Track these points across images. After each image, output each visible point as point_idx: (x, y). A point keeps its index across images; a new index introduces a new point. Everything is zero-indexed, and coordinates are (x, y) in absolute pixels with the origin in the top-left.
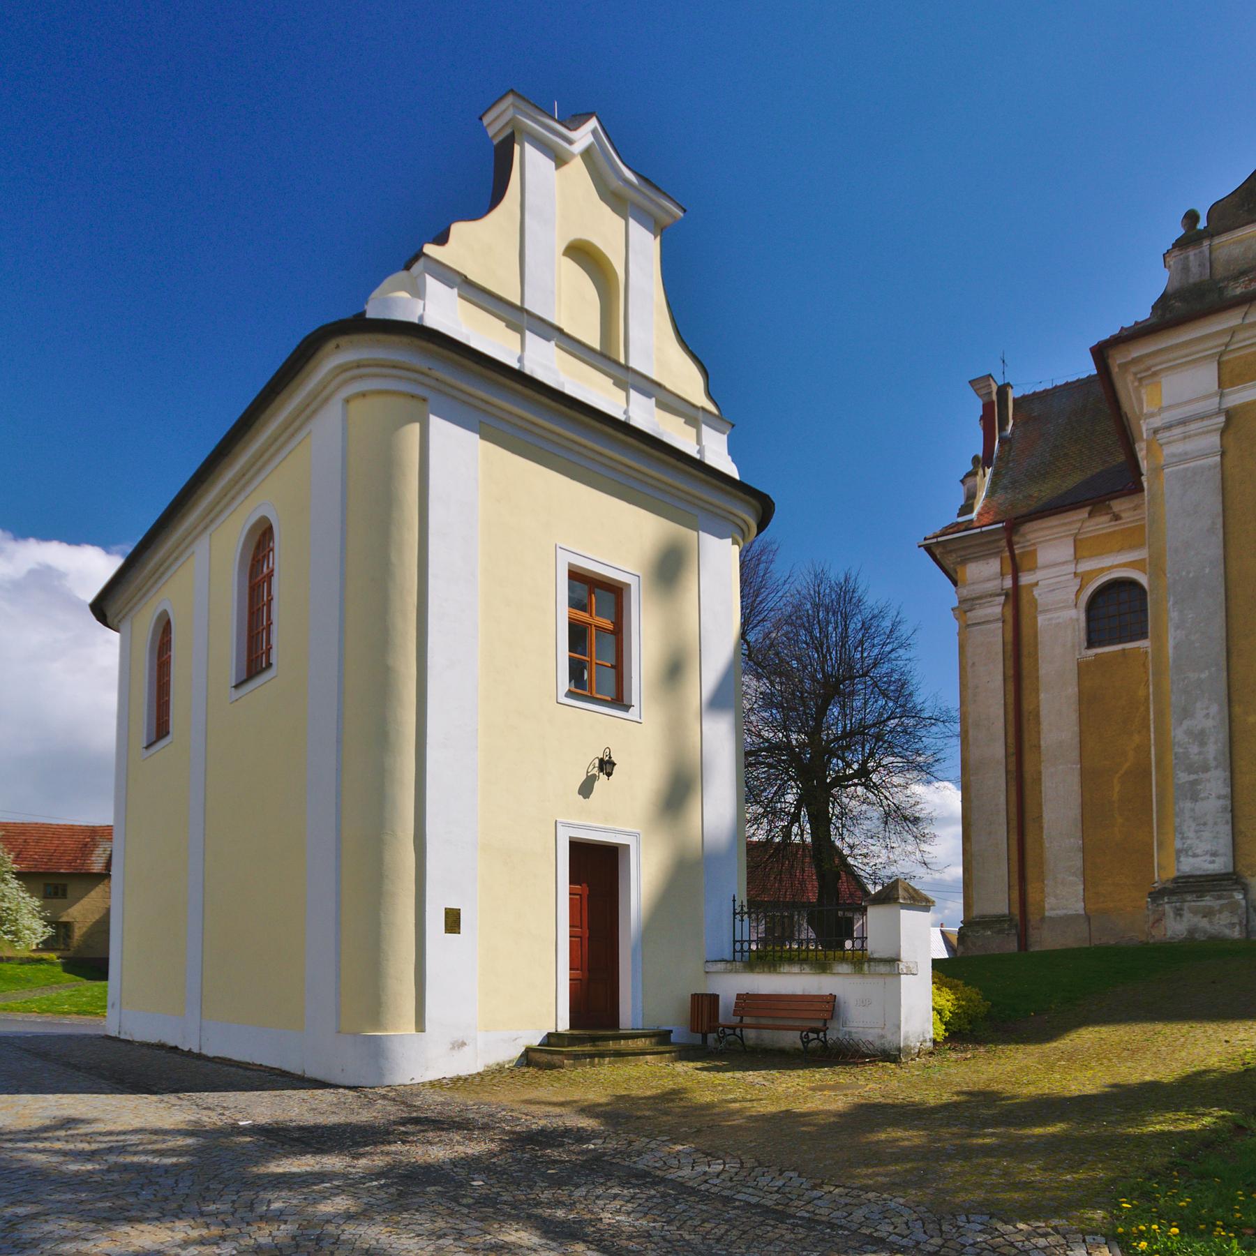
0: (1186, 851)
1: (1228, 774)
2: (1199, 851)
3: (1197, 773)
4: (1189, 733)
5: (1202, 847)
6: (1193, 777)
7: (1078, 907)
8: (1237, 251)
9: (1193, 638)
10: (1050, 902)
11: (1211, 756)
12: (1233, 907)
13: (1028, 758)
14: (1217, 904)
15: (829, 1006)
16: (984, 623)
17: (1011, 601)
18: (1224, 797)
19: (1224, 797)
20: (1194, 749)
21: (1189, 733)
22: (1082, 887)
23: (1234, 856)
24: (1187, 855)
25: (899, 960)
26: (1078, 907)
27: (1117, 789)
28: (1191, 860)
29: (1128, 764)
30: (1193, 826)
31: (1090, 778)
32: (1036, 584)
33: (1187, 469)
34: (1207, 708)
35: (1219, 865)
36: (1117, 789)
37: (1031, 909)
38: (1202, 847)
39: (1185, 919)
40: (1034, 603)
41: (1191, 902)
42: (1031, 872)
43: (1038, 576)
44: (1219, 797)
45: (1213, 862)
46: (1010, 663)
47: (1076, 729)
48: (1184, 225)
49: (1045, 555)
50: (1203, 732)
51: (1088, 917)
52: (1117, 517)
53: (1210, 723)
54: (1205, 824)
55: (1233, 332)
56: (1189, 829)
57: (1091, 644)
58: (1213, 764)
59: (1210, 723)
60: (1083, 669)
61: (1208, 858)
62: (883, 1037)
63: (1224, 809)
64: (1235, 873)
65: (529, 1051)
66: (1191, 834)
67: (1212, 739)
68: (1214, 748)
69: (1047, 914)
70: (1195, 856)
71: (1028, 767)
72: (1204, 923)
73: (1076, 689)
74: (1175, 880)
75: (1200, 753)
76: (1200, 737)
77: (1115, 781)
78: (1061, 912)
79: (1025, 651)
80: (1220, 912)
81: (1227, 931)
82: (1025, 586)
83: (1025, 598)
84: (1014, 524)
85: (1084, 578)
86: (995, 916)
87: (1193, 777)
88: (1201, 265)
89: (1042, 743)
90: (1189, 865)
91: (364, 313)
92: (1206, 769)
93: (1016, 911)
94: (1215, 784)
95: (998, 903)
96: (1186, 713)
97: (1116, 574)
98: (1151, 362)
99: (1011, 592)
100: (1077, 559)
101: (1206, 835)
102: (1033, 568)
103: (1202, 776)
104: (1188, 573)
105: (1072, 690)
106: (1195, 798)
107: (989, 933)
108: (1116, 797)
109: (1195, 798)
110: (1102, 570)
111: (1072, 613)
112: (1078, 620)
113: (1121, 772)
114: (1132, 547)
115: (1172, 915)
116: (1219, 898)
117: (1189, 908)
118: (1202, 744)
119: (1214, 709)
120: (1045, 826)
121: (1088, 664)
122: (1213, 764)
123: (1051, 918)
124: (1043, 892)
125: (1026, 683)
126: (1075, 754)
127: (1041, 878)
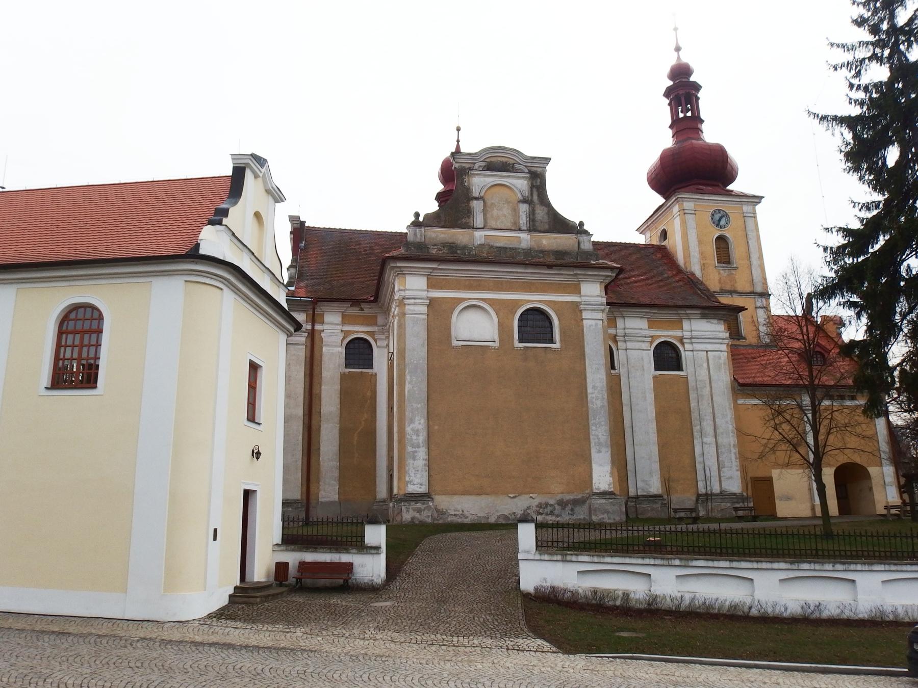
0: (411, 482)
1: (427, 450)
2: (415, 483)
3: (415, 448)
4: (412, 430)
5: (416, 481)
6: (414, 449)
7: (335, 497)
8: (434, 235)
9: (415, 389)
10: (322, 494)
11: (421, 442)
12: (429, 508)
13: (314, 417)
14: (423, 507)
15: (349, 567)
16: (296, 344)
17: (310, 335)
18: (426, 460)
19: (426, 460)
20: (414, 437)
21: (412, 430)
22: (338, 487)
23: (429, 486)
24: (411, 484)
25: (380, 548)
26: (335, 497)
27: (356, 439)
28: (412, 487)
29: (361, 428)
30: (413, 471)
31: (345, 433)
32: (323, 331)
33: (414, 317)
34: (420, 420)
35: (423, 489)
36: (356, 439)
37: (312, 497)
38: (416, 481)
39: (410, 513)
40: (322, 339)
41: (413, 505)
42: (312, 478)
43: (325, 327)
44: (423, 460)
45: (421, 488)
46: (308, 367)
47: (339, 407)
48: (414, 216)
49: (328, 318)
50: (418, 430)
51: (340, 502)
52: (362, 310)
53: (420, 427)
54: (418, 471)
55: (434, 269)
56: (412, 472)
57: (347, 366)
58: (421, 445)
59: (420, 427)
60: (343, 377)
61: (419, 486)
62: (372, 580)
63: (425, 465)
64: (429, 493)
65: (230, 596)
66: (412, 475)
67: (421, 434)
68: (422, 438)
69: (320, 500)
70: (414, 485)
71: (314, 422)
72: (417, 515)
73: (339, 387)
74: (405, 495)
75: (417, 439)
76: (417, 432)
77: (356, 435)
78: (327, 500)
79: (316, 363)
80: (424, 510)
81: (426, 519)
82: (318, 330)
83: (317, 336)
84: (316, 302)
85: (346, 333)
86: (294, 500)
87: (414, 449)
88: (421, 236)
89: (322, 411)
90: (412, 489)
91: (197, 246)
92: (419, 447)
93: (304, 498)
94: (422, 453)
95: (297, 494)
96: (412, 421)
97: (359, 336)
98: (402, 269)
99: (310, 332)
100: (343, 323)
101: (418, 476)
102: (322, 323)
103: (417, 449)
104: (414, 361)
105: (338, 387)
106: (414, 459)
107: (290, 509)
108: (355, 443)
109: (414, 459)
110: (354, 332)
111: (339, 349)
112: (341, 353)
113: (359, 430)
114: (367, 325)
115: (405, 511)
116: (423, 504)
117: (412, 508)
118: (418, 435)
119: (422, 421)
120: (321, 454)
121: (345, 375)
122: (421, 445)
123: (322, 502)
124: (318, 488)
125: (315, 380)
126: (337, 419)
127: (318, 481)
